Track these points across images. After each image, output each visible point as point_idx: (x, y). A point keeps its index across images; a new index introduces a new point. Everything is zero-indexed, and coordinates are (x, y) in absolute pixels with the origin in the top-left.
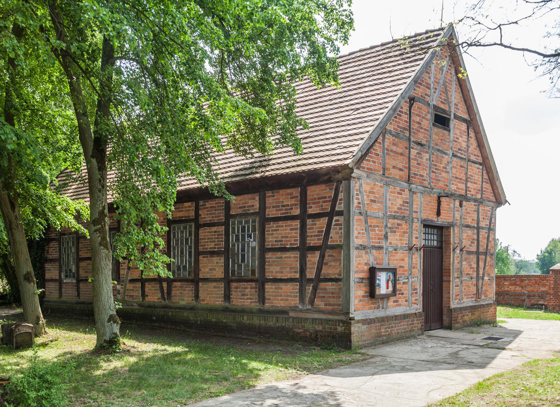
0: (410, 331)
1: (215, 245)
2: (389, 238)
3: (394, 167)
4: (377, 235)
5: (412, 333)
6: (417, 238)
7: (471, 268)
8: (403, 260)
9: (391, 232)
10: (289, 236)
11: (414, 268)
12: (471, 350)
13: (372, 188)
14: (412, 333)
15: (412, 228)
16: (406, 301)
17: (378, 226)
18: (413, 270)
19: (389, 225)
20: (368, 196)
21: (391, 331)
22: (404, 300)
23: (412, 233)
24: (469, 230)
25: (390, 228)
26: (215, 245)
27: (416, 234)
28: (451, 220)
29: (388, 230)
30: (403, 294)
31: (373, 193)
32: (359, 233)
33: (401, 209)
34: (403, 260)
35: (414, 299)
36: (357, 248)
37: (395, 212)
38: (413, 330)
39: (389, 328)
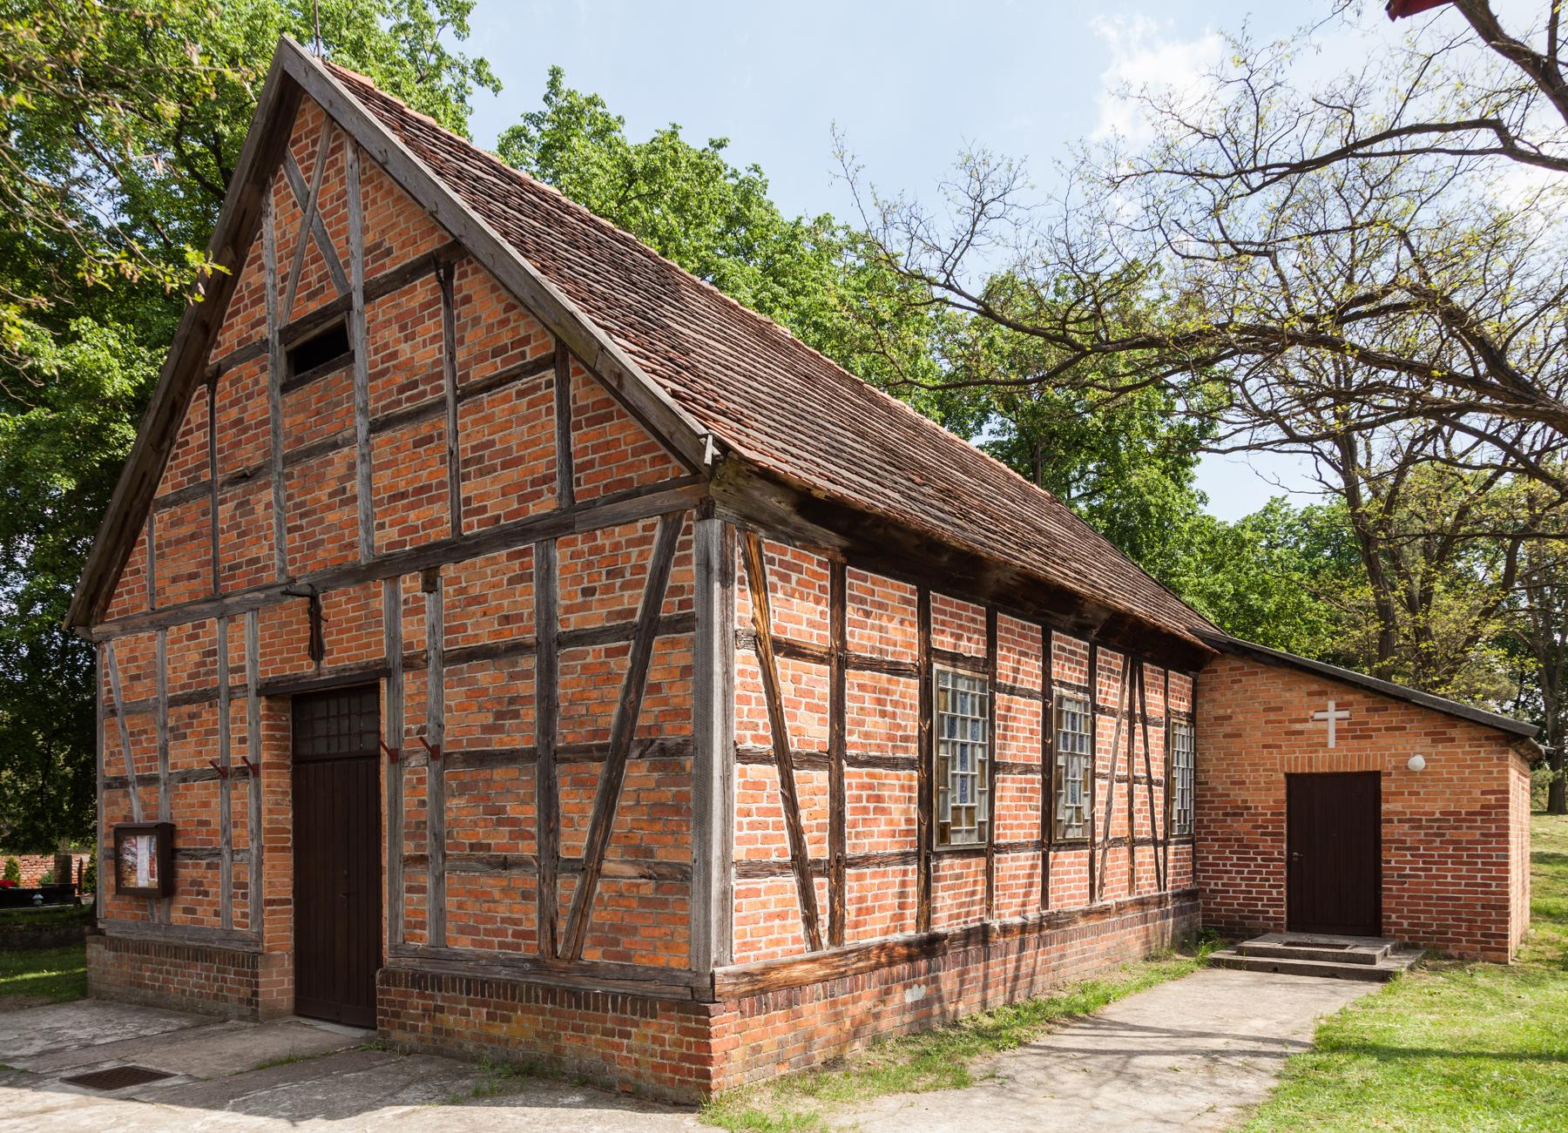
0: (216, 997)
1: (321, 521)
2: (172, 753)
3: (175, 580)
4: (145, 751)
5: (222, 1006)
6: (243, 741)
7: (500, 823)
8: (206, 805)
9: (176, 738)
10: (434, 482)
11: (235, 825)
12: (57, 1118)
13: (132, 650)
14: (222, 1006)
15: (227, 716)
16: (217, 914)
17: (145, 732)
18: (234, 832)
19: (171, 723)
20: (125, 671)
21: (166, 981)
22: (211, 910)
23: (227, 728)
24: (483, 668)
25: (172, 729)
26: (321, 521)
27: (241, 731)
28: (379, 651)
29: (168, 735)
30: (206, 894)
31: (135, 659)
32: (112, 754)
33: (197, 675)
34: (206, 805)
35: (238, 911)
36: (108, 786)
37: (183, 687)
38: (225, 999)
39: (161, 972)
